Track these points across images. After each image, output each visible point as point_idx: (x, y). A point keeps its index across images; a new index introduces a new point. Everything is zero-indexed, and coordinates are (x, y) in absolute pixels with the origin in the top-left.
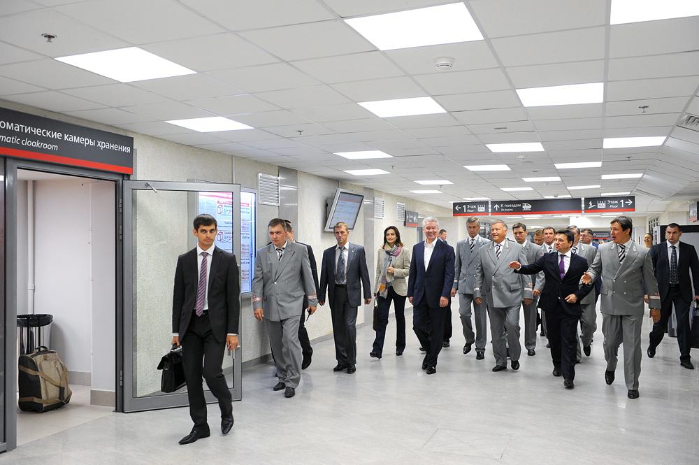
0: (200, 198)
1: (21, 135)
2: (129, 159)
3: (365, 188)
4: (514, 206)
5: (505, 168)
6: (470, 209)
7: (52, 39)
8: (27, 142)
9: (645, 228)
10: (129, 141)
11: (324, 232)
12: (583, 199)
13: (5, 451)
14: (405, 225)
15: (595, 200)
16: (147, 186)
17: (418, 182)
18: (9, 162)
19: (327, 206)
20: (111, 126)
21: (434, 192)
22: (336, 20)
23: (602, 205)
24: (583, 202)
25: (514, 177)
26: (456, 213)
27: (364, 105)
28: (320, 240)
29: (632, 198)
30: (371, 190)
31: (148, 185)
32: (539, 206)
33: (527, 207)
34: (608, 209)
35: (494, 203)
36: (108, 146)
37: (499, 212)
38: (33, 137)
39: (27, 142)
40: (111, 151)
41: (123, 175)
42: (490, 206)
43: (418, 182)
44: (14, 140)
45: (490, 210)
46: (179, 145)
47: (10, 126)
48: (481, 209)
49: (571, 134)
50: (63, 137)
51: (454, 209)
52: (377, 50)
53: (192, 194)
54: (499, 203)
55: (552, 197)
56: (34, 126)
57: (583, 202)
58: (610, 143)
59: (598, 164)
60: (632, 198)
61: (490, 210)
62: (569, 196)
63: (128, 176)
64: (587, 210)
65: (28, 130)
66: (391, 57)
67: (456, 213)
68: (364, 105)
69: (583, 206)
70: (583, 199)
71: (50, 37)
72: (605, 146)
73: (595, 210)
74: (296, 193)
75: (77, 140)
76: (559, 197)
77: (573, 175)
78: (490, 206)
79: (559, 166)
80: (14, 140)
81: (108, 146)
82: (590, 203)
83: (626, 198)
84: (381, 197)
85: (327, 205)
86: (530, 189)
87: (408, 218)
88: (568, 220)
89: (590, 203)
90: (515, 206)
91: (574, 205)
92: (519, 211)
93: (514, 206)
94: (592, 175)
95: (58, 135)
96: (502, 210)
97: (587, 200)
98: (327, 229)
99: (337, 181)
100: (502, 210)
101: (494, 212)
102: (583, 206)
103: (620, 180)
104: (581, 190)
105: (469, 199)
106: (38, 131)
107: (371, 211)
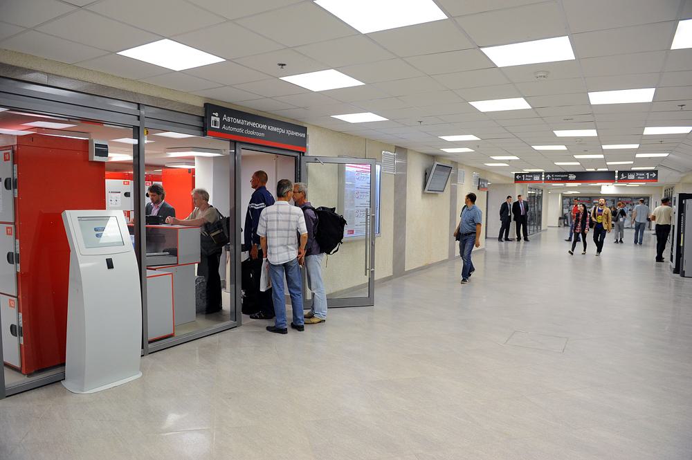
0: (346, 167)
1: (245, 127)
2: (303, 142)
3: (452, 162)
4: (563, 176)
5: (563, 148)
6: (528, 178)
7: (284, 67)
8: (248, 132)
9: (661, 195)
10: (304, 130)
11: (423, 193)
12: (617, 172)
13: (143, 348)
14: (478, 189)
15: (626, 173)
16: (316, 160)
17: (442, 137)
18: (237, 145)
19: (426, 175)
20: (294, 120)
21: (502, 162)
22: (474, 49)
23: (631, 177)
24: (617, 174)
25: (567, 156)
26: (516, 181)
27: (471, 103)
28: (420, 197)
29: (656, 172)
30: (456, 163)
31: (316, 159)
32: (582, 176)
33: (572, 177)
34: (636, 180)
35: (546, 174)
36: (293, 133)
37: (551, 181)
38: (251, 128)
39: (248, 132)
40: (295, 136)
41: (300, 152)
42: (543, 176)
43: (442, 137)
44: (240, 130)
45: (543, 179)
46: (334, 132)
47: (238, 121)
48: (537, 178)
49: (624, 121)
50: (267, 128)
51: (516, 178)
52: (497, 67)
53: (341, 167)
54: (550, 174)
55: (593, 170)
56: (295, 131)
57: (617, 174)
58: (649, 131)
59: (636, 146)
60: (656, 172)
61: (543, 179)
62: (607, 170)
63: (303, 153)
64: (619, 181)
65: (249, 123)
66: (536, 150)
67: (516, 181)
68: (471, 103)
69: (616, 177)
70: (617, 172)
71: (282, 65)
72: (645, 133)
73: (626, 180)
74: (406, 165)
75: (275, 129)
76: (599, 170)
77: (620, 151)
78: (543, 176)
79: (605, 147)
80: (240, 130)
81: (293, 133)
82: (623, 175)
83: (651, 172)
84: (462, 168)
85: (426, 174)
86: (578, 164)
87: (480, 184)
88: (600, 188)
89: (623, 175)
90: (563, 177)
91: (609, 176)
92: (566, 180)
93: (563, 176)
94: (629, 154)
95: (264, 127)
96: (553, 179)
97: (620, 173)
98: (426, 191)
99: (433, 157)
100: (553, 179)
101: (546, 180)
102: (616, 177)
103: (650, 158)
104: (616, 164)
105: (527, 171)
106: (254, 124)
107: (455, 180)
